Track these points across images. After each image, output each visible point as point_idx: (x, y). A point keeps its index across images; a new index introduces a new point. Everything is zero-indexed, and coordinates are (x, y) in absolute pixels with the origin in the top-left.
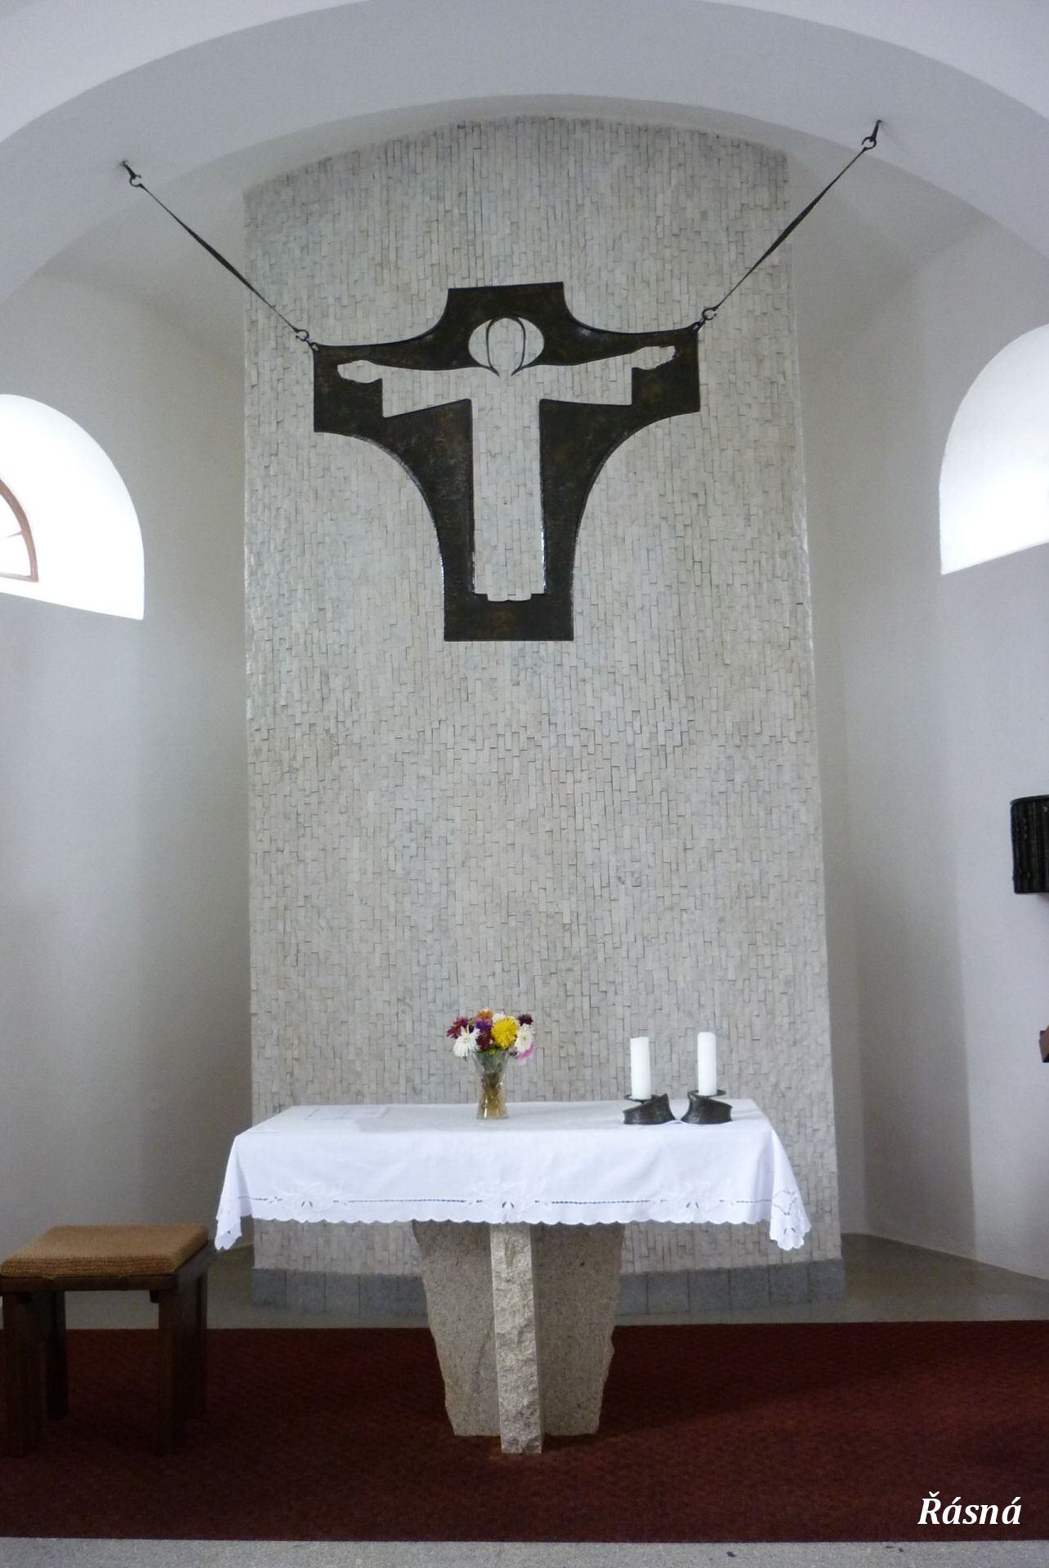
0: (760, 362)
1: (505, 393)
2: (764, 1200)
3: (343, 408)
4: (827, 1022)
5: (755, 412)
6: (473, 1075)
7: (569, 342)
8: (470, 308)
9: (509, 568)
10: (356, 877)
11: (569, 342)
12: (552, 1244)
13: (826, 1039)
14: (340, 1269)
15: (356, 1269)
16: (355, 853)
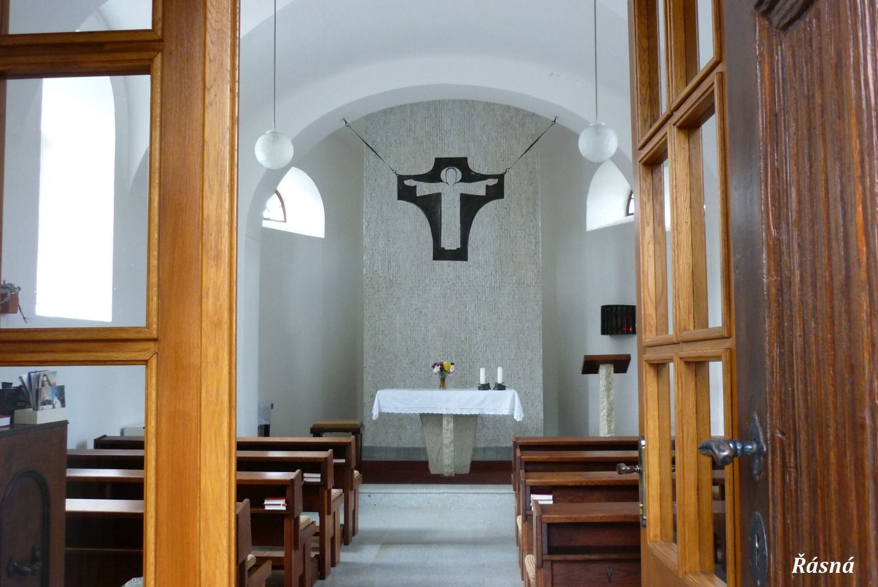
0: (528, 165)
1: (451, 190)
2: (513, 409)
3: (406, 193)
4: (541, 373)
5: (525, 182)
6: (437, 380)
7: (469, 176)
8: (441, 164)
9: (450, 241)
10: (398, 325)
11: (469, 176)
12: (459, 420)
13: (541, 378)
14: (391, 445)
15: (396, 445)
16: (398, 318)
